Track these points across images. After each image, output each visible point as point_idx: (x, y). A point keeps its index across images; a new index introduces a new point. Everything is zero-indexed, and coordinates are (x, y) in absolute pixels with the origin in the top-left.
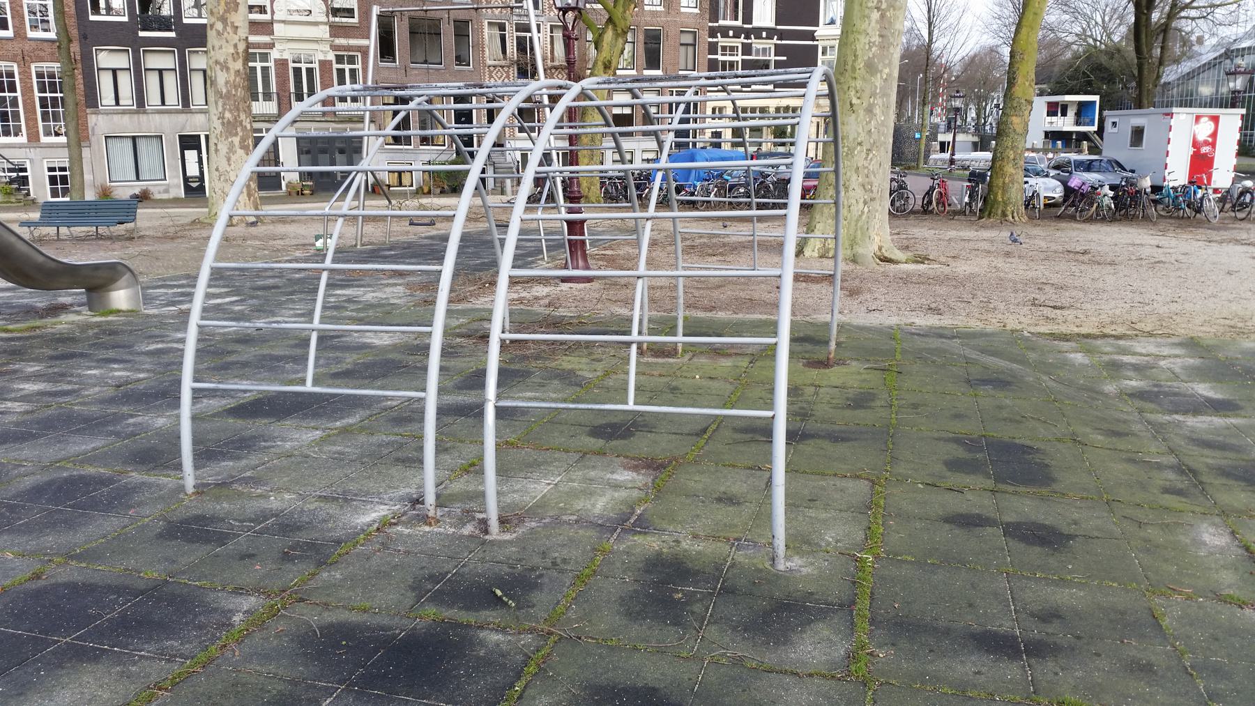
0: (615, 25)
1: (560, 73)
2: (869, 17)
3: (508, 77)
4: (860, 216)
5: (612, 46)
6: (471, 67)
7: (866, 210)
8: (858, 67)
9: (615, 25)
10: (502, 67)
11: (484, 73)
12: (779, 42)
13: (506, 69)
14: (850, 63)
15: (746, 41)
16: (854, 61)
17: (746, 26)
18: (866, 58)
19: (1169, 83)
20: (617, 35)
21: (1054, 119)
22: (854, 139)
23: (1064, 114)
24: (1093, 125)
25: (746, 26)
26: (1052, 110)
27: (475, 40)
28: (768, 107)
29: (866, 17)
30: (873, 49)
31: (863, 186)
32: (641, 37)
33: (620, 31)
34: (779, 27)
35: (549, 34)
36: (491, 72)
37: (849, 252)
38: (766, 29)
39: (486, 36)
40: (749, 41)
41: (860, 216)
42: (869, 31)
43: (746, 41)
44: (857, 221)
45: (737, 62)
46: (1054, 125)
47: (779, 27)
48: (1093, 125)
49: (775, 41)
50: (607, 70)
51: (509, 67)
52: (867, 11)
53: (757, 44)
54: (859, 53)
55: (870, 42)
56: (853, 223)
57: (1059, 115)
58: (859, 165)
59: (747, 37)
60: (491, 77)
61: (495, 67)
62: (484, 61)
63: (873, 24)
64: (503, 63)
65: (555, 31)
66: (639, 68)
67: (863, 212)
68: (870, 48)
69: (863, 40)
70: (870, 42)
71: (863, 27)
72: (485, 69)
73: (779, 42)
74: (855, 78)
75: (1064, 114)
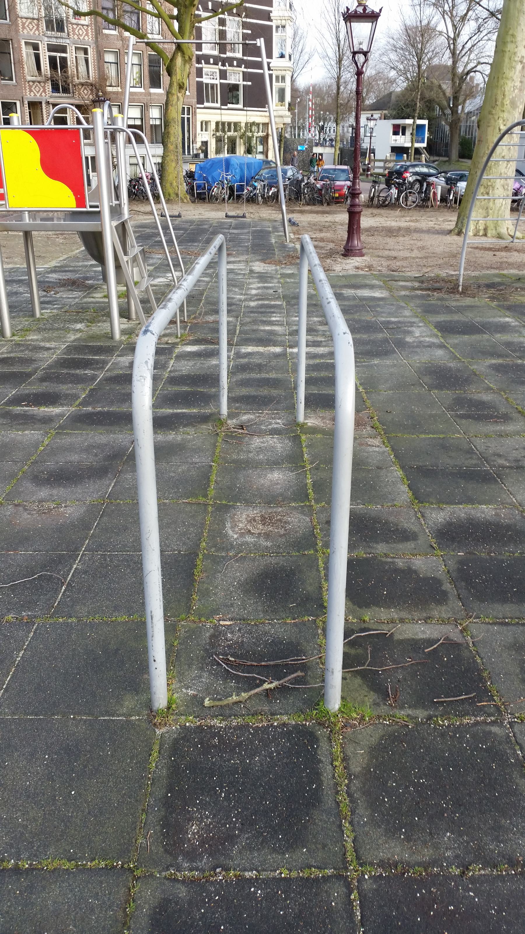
0: (183, 53)
1: (85, 89)
2: (515, 68)
3: (44, 91)
4: (501, 207)
5: (183, 70)
6: (14, 81)
7: (504, 203)
8: (505, 104)
9: (183, 53)
10: (39, 82)
11: (25, 88)
12: (245, 70)
13: (43, 84)
14: (500, 100)
15: (222, 68)
16: (503, 99)
17: (222, 55)
18: (511, 97)
19: (471, 112)
20: (185, 62)
21: (398, 137)
22: (500, 154)
23: (404, 134)
24: (424, 142)
25: (222, 55)
26: (397, 130)
27: (16, 57)
28: (240, 123)
29: (513, 68)
30: (516, 91)
31: (503, 186)
32: (146, 61)
33: (187, 58)
34: (245, 58)
35: (74, 55)
36: (30, 87)
37: (494, 232)
38: (213, 57)
39: (24, 55)
40: (225, 68)
41: (501, 207)
42: (515, 78)
43: (222, 68)
44: (499, 210)
45: (217, 85)
46: (397, 142)
47: (245, 58)
48: (424, 142)
49: (243, 69)
50: (181, 90)
51: (45, 82)
52: (514, 64)
53: (207, 69)
54: (507, 93)
55: (514, 86)
56: (496, 212)
57: (401, 134)
58: (502, 171)
59: (223, 65)
60: (31, 91)
61: (34, 82)
62: (24, 76)
63: (517, 73)
64: (39, 79)
65: (77, 52)
66: (146, 86)
67: (502, 205)
68: (514, 90)
69: (510, 84)
70: (514, 86)
71: (510, 75)
72: (25, 84)
73: (245, 70)
74: (504, 111)
75: (404, 134)
